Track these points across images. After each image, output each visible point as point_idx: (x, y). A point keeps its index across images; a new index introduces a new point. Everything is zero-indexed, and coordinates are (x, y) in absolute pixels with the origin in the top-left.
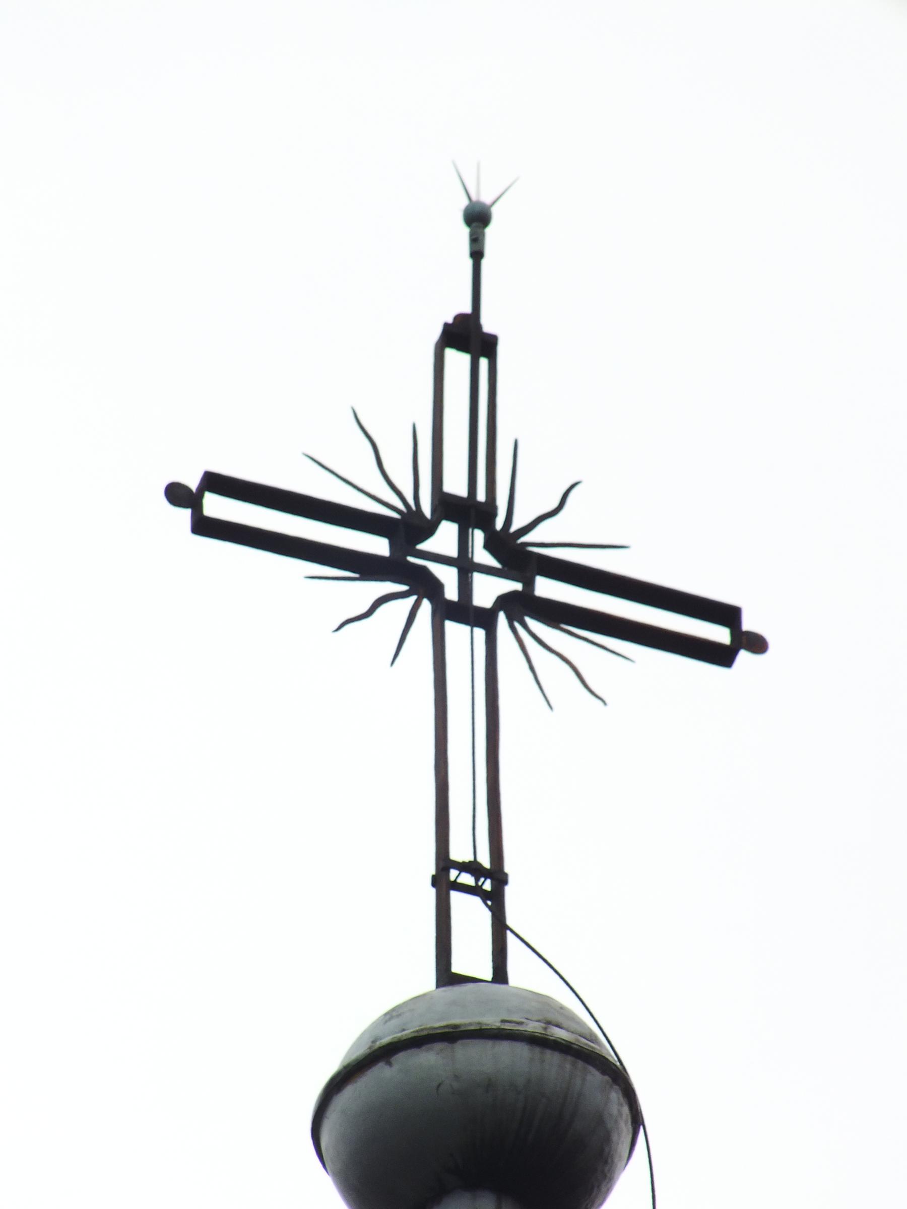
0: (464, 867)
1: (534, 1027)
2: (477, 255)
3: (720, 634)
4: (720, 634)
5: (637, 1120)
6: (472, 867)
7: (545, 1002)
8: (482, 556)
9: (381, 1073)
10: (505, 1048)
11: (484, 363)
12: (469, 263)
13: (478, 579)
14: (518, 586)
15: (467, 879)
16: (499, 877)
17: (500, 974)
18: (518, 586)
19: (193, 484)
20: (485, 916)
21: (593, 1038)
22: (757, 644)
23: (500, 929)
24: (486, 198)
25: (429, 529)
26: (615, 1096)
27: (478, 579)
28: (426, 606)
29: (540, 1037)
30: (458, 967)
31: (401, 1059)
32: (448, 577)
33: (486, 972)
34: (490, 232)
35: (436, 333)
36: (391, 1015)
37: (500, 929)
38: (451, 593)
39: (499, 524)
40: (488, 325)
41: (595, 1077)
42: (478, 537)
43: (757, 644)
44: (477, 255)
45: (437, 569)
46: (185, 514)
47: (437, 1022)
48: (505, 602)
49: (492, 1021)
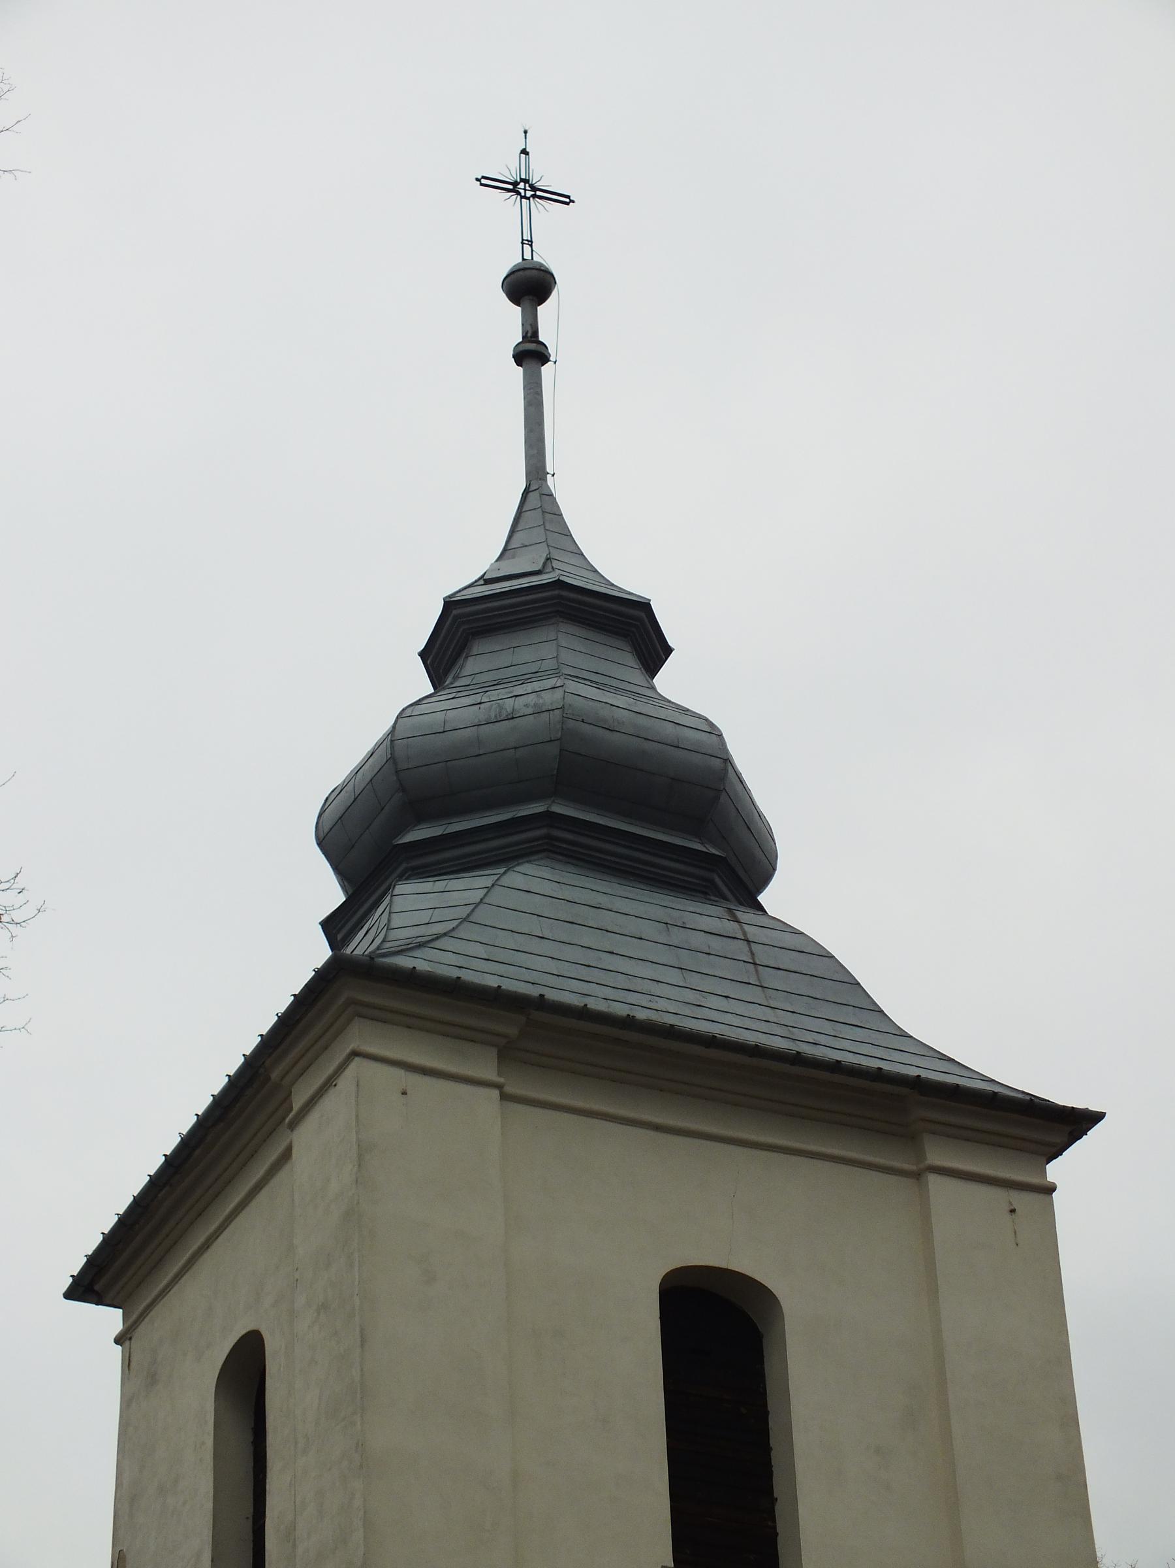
0: (526, 240)
1: (538, 267)
2: (526, 138)
3: (567, 200)
4: (567, 200)
5: (555, 283)
6: (527, 240)
7: (540, 263)
8: (528, 188)
9: (512, 276)
10: (534, 271)
11: (511, 187)
12: (524, 140)
13: (527, 192)
14: (533, 193)
15: (527, 242)
16: (531, 241)
17: (532, 259)
18: (533, 193)
19: (480, 177)
20: (530, 248)
21: (548, 269)
22: (573, 202)
23: (532, 251)
24: (527, 129)
25: (519, 184)
26: (552, 279)
27: (527, 192)
28: (519, 197)
29: (1020, 1098)
30: (525, 257)
31: (516, 274)
32: (522, 192)
33: (530, 258)
34: (527, 134)
35: (519, 152)
36: (514, 266)
37: (532, 251)
38: (523, 194)
39: (530, 183)
40: (528, 150)
41: (549, 276)
42: (527, 185)
43: (573, 202)
44: (526, 138)
45: (520, 190)
46: (479, 182)
47: (522, 267)
48: (532, 196)
49: (531, 266)
